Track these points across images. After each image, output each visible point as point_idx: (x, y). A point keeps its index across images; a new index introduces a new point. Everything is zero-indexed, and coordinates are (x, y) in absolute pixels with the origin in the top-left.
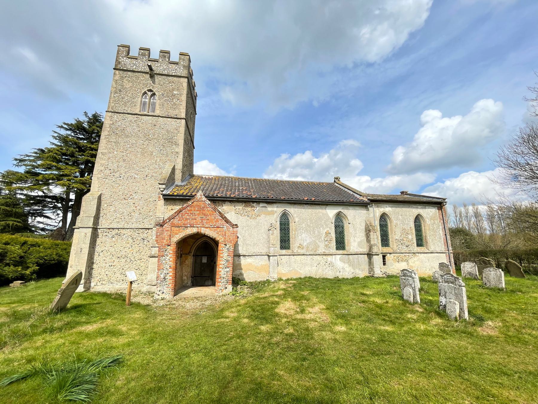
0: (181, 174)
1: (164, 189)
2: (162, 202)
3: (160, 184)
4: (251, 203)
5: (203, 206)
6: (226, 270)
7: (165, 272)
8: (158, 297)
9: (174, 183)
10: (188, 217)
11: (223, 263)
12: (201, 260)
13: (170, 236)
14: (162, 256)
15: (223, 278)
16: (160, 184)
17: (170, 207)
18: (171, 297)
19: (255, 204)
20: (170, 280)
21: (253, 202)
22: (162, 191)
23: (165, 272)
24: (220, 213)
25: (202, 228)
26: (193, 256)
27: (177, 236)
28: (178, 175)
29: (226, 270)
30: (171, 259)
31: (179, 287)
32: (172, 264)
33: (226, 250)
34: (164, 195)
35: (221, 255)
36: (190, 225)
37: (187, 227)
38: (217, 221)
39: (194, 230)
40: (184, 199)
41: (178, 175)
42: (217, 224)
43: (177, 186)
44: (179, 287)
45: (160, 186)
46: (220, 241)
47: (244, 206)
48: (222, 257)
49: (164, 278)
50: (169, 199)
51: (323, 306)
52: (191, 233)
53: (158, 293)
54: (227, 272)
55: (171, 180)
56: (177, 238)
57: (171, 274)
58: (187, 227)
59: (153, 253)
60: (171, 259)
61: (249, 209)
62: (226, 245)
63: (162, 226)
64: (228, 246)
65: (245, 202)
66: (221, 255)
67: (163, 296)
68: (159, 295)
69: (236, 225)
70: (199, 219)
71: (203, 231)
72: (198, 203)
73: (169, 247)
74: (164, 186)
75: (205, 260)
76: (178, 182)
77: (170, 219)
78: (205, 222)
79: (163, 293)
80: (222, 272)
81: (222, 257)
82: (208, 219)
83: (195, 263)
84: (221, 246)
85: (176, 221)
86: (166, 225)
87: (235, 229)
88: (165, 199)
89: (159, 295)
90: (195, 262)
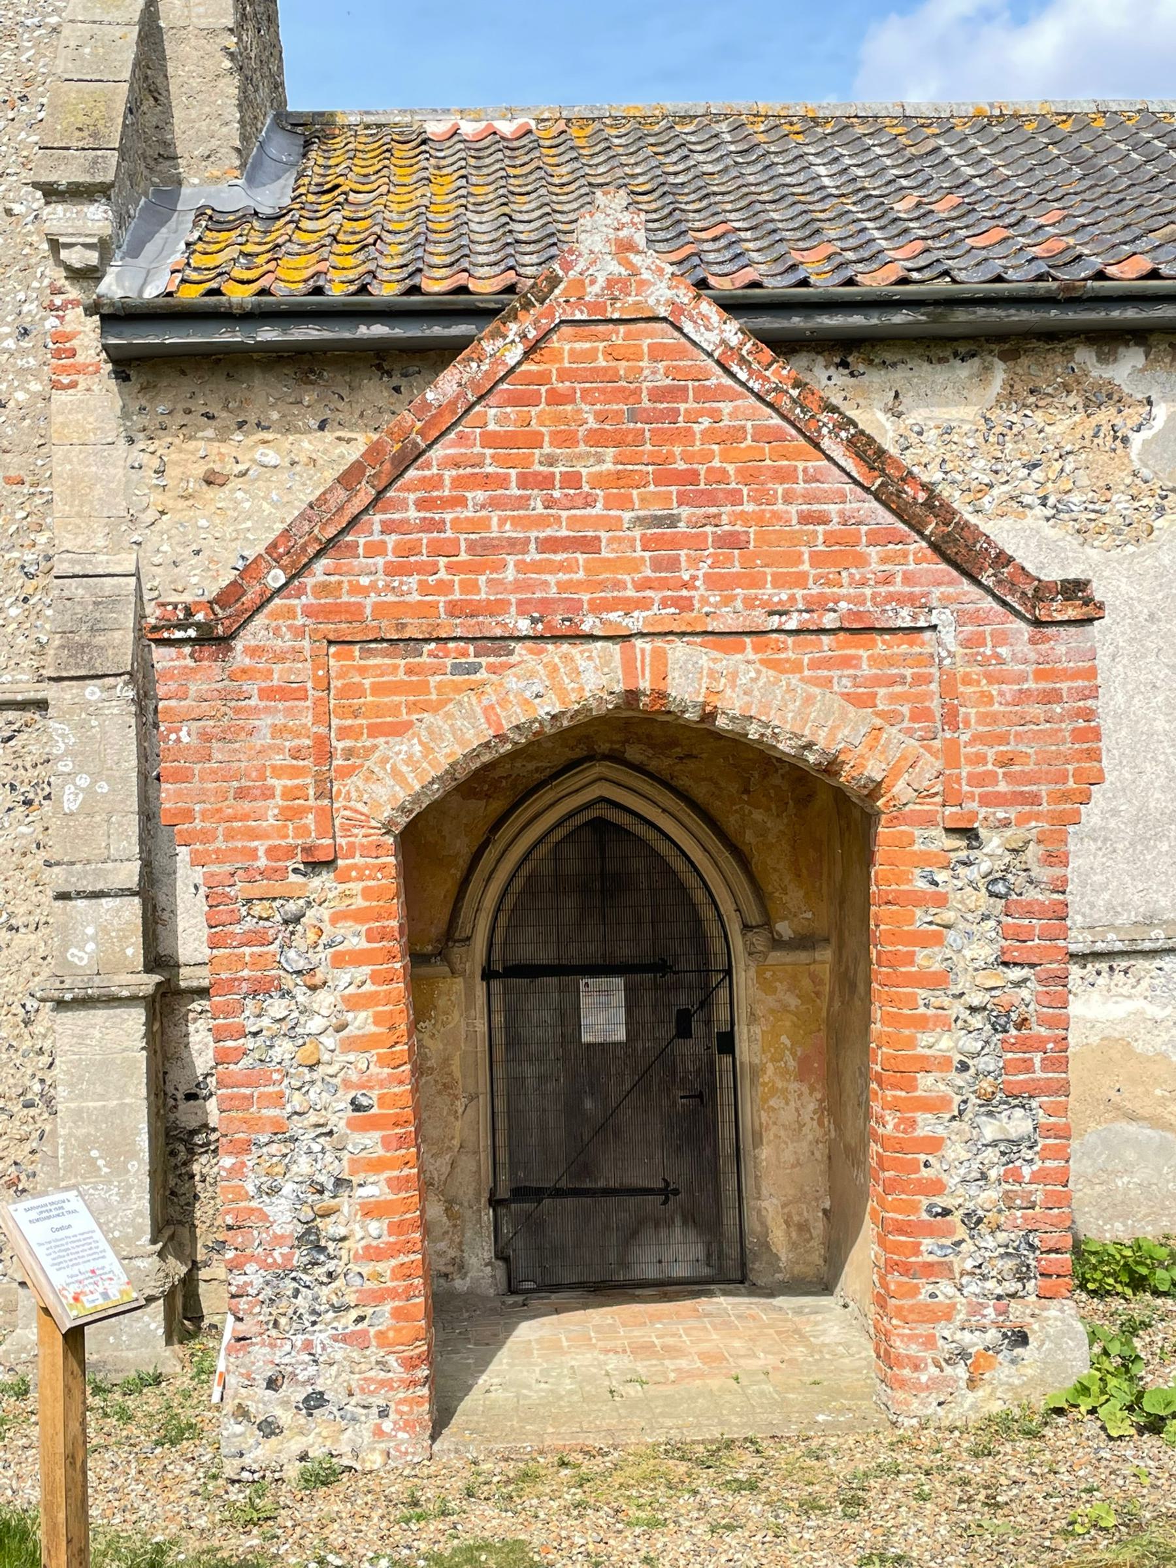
0: (230, 87)
1: (104, 247)
2: (97, 397)
3: (51, 193)
4: (1084, 356)
5: (654, 375)
6: (990, 1130)
7: (303, 1166)
8: (260, 1452)
9: (167, 197)
10: (498, 527)
11: (946, 1044)
12: (570, 1017)
13: (323, 751)
14: (261, 989)
15: (973, 1221)
16: (51, 193)
17: (194, 452)
18: (409, 1444)
19: (1126, 369)
20: (373, 1254)
21: (1109, 339)
22: (87, 275)
23: (303, 1166)
24: (866, 449)
25: (678, 650)
26: (488, 974)
27: (402, 748)
28: (205, 107)
29: (990, 1130)
30: (361, 1022)
31: (456, 1330)
32: (383, 1077)
33: (980, 900)
34: (115, 317)
35: (928, 959)
36: (539, 610)
37: (502, 642)
38: (842, 551)
39: (587, 679)
40: (373, 346)
41: (205, 107)
42: (848, 596)
43: (213, 220)
44: (456, 1330)
45: (59, 217)
46: (900, 789)
47: (1010, 395)
48: (937, 981)
49: (311, 1239)
50: (175, 356)
51: (678, 1230)
52: (548, 706)
53: (262, 1403)
54: (1010, 1147)
55: (145, 165)
56: (401, 771)
57: (375, 1189)
58: (502, 642)
59: (82, 956)
60: (361, 1022)
61: (1061, 423)
62: (969, 834)
63: (212, 640)
64: (993, 843)
65: (1009, 344)
66: (928, 959)
67: (317, 1438)
68: (269, 1428)
69: (1074, 589)
70: (623, 537)
71: (692, 679)
72: (594, 349)
73: (322, 881)
74: (96, 218)
75: (604, 1015)
76: (210, 176)
77: (299, 553)
78: (694, 569)
79: (315, 1402)
80: (955, 1151)
81: (937, 981)
82: (731, 541)
83: (508, 1042)
84: (910, 860)
85: (366, 577)
86: (256, 632)
87: (1064, 645)
88: (126, 365)
89: (269, 1428)
90: (513, 1040)
